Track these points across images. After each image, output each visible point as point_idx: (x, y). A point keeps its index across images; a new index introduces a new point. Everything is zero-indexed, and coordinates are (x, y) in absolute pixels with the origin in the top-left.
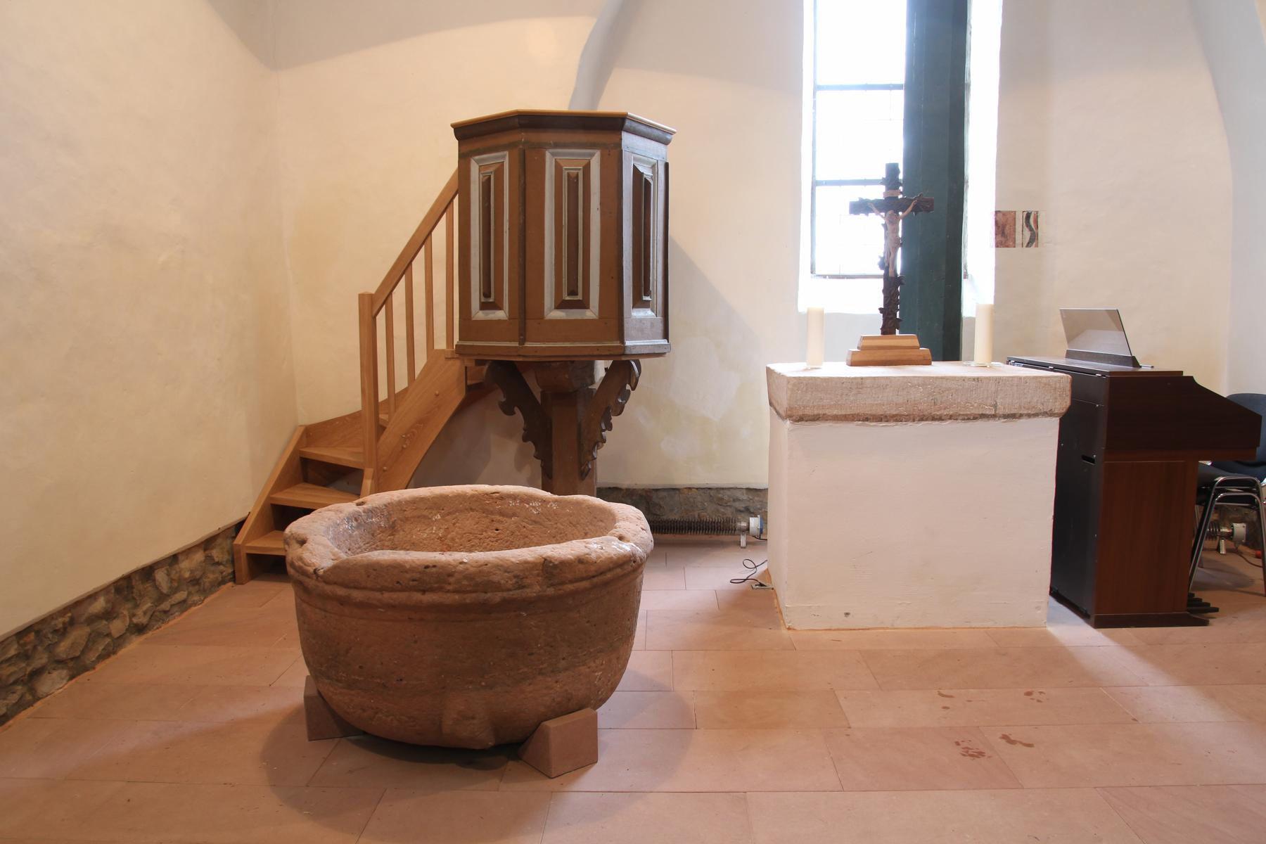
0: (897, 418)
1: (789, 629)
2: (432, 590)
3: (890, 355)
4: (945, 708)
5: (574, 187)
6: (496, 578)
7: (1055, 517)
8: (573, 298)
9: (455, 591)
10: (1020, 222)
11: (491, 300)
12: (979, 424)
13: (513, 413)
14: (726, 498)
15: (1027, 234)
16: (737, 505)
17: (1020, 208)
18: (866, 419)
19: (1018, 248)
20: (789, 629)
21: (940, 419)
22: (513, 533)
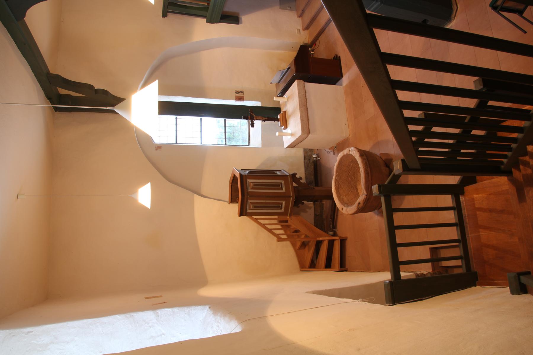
0: (308, 113)
1: (349, 136)
2: (368, 172)
3: (284, 119)
4: (368, 100)
5: (257, 185)
6: (365, 162)
7: (323, 84)
8: (279, 186)
9: (368, 168)
10: (238, 95)
11: (280, 205)
12: (307, 98)
13: (303, 203)
14: (307, 165)
15: (241, 93)
16: (308, 163)
17: (234, 95)
18: (308, 119)
19: (244, 95)
20: (349, 136)
21: (307, 105)
22: (342, 183)
